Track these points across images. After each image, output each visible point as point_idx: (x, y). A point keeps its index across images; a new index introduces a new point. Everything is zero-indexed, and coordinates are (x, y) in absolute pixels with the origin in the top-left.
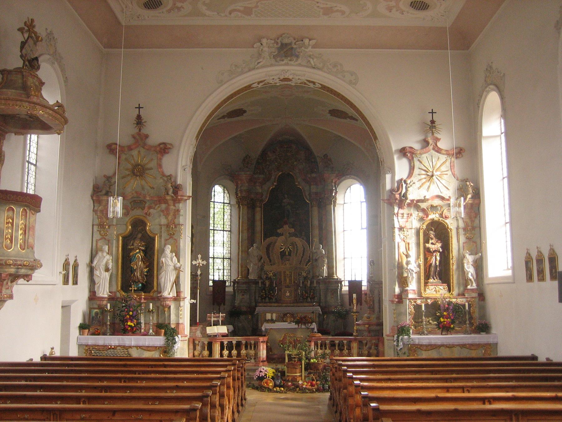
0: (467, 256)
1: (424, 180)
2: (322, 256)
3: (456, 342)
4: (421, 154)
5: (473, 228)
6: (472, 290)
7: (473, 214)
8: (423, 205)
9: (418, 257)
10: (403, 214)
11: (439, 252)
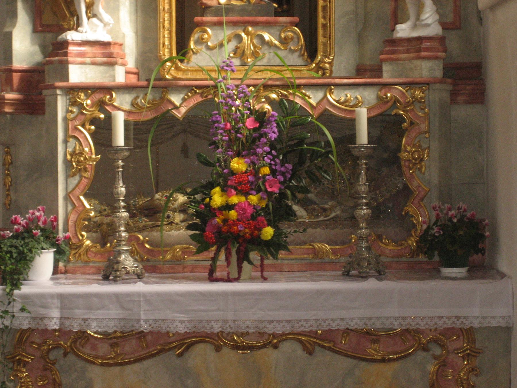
3: (276, 319)
6: (415, 44)
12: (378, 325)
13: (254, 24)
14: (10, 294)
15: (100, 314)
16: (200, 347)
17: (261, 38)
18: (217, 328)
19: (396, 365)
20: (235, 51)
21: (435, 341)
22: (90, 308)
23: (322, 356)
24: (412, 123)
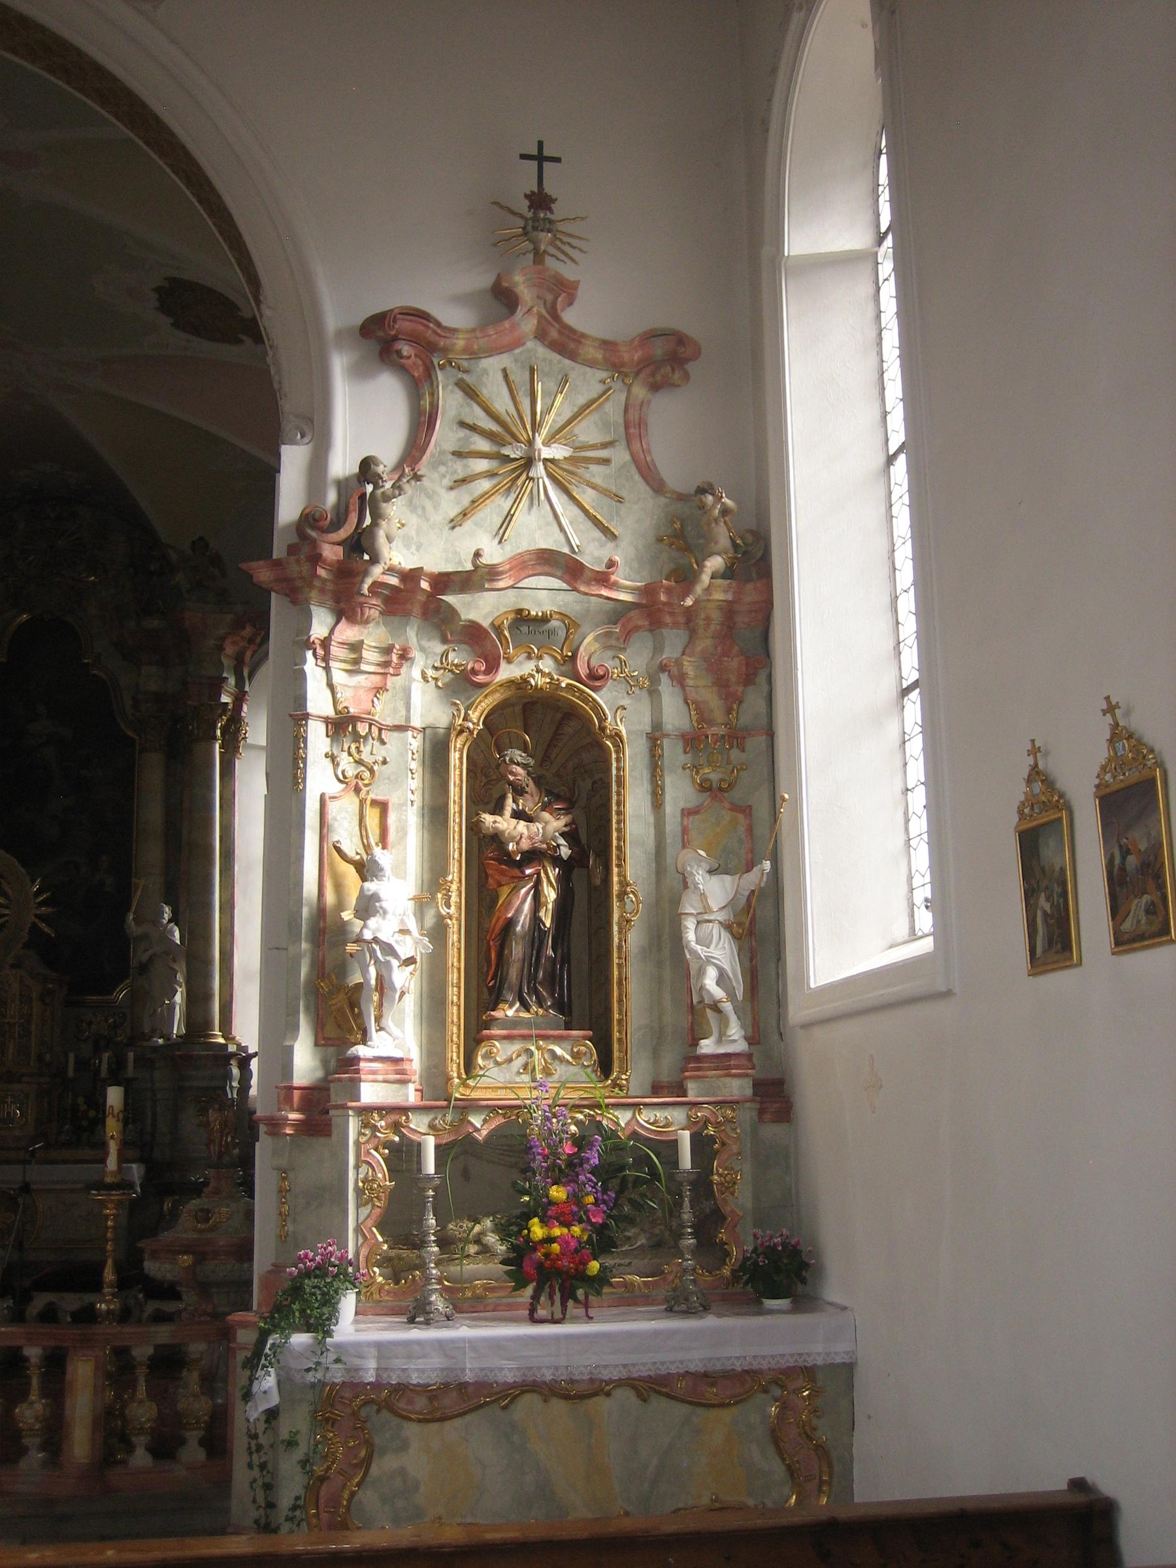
0: (700, 877)
1: (485, 485)
2: (167, 953)
3: (611, 1365)
4: (474, 355)
5: (736, 737)
6: (722, 1061)
7: (734, 664)
8: (480, 608)
9: (435, 879)
10: (356, 647)
11: (557, 861)
12: (718, 1367)
13: (545, 1038)
14: (321, 1343)
15: (421, 1363)
16: (528, 1398)
17: (552, 1052)
18: (548, 1376)
19: (734, 1410)
20: (525, 1067)
21: (776, 1382)
22: (409, 1357)
23: (659, 1404)
24: (723, 1144)
